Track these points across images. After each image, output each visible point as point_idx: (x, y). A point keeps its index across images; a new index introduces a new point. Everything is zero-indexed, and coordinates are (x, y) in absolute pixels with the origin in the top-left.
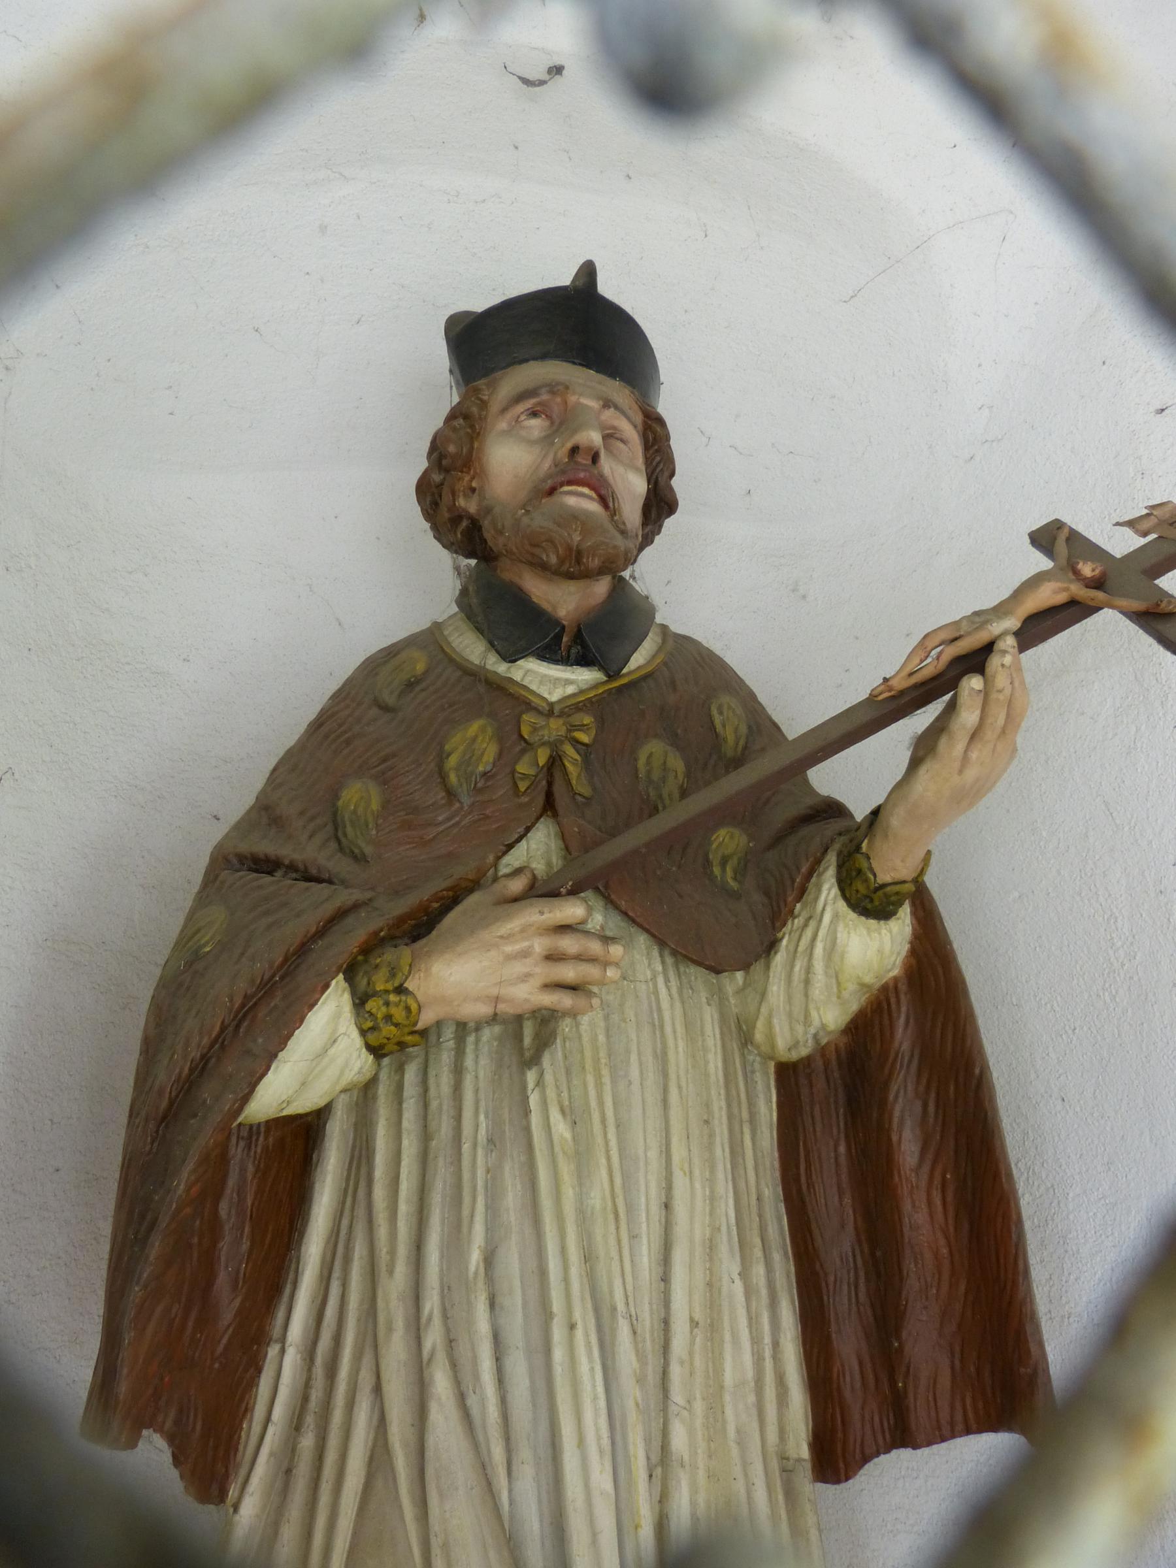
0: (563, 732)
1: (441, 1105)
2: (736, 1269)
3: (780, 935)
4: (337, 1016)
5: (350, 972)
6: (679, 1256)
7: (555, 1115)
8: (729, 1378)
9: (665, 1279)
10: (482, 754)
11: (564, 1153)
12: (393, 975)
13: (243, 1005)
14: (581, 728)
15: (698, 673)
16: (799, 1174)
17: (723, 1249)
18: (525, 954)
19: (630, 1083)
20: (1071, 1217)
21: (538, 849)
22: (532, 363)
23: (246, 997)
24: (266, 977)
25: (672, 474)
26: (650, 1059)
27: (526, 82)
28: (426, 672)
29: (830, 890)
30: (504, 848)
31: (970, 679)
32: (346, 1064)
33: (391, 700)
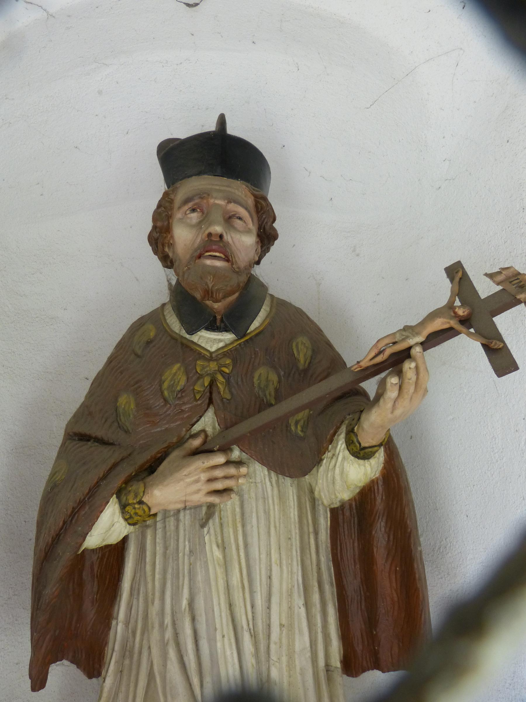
0: (217, 369)
1: (170, 534)
2: (301, 602)
3: (323, 457)
4: (113, 514)
5: (119, 493)
6: (275, 600)
7: (215, 547)
8: (298, 647)
9: (269, 608)
10: (179, 382)
11: (219, 564)
12: (136, 496)
13: (72, 512)
14: (225, 366)
15: (292, 320)
16: (337, 553)
17: (296, 596)
18: (197, 481)
19: (252, 527)
20: (468, 567)
21: (209, 421)
22: (194, 177)
23: (74, 509)
24: (81, 500)
25: (274, 220)
26: (263, 514)
27: (188, 5)
28: (156, 336)
29: (342, 444)
30: (190, 427)
31: (391, 378)
32: (121, 532)
33: (139, 352)
